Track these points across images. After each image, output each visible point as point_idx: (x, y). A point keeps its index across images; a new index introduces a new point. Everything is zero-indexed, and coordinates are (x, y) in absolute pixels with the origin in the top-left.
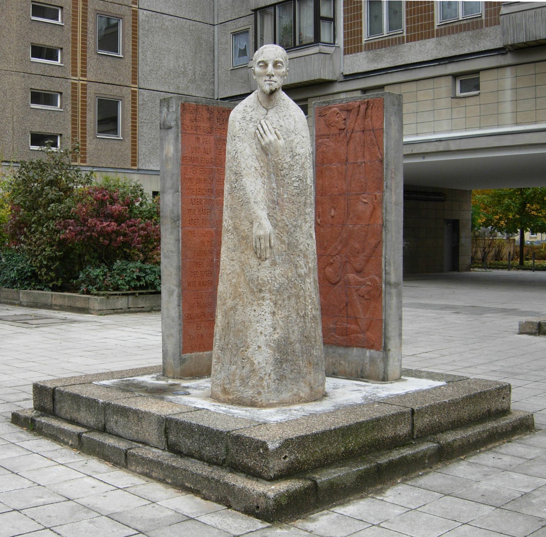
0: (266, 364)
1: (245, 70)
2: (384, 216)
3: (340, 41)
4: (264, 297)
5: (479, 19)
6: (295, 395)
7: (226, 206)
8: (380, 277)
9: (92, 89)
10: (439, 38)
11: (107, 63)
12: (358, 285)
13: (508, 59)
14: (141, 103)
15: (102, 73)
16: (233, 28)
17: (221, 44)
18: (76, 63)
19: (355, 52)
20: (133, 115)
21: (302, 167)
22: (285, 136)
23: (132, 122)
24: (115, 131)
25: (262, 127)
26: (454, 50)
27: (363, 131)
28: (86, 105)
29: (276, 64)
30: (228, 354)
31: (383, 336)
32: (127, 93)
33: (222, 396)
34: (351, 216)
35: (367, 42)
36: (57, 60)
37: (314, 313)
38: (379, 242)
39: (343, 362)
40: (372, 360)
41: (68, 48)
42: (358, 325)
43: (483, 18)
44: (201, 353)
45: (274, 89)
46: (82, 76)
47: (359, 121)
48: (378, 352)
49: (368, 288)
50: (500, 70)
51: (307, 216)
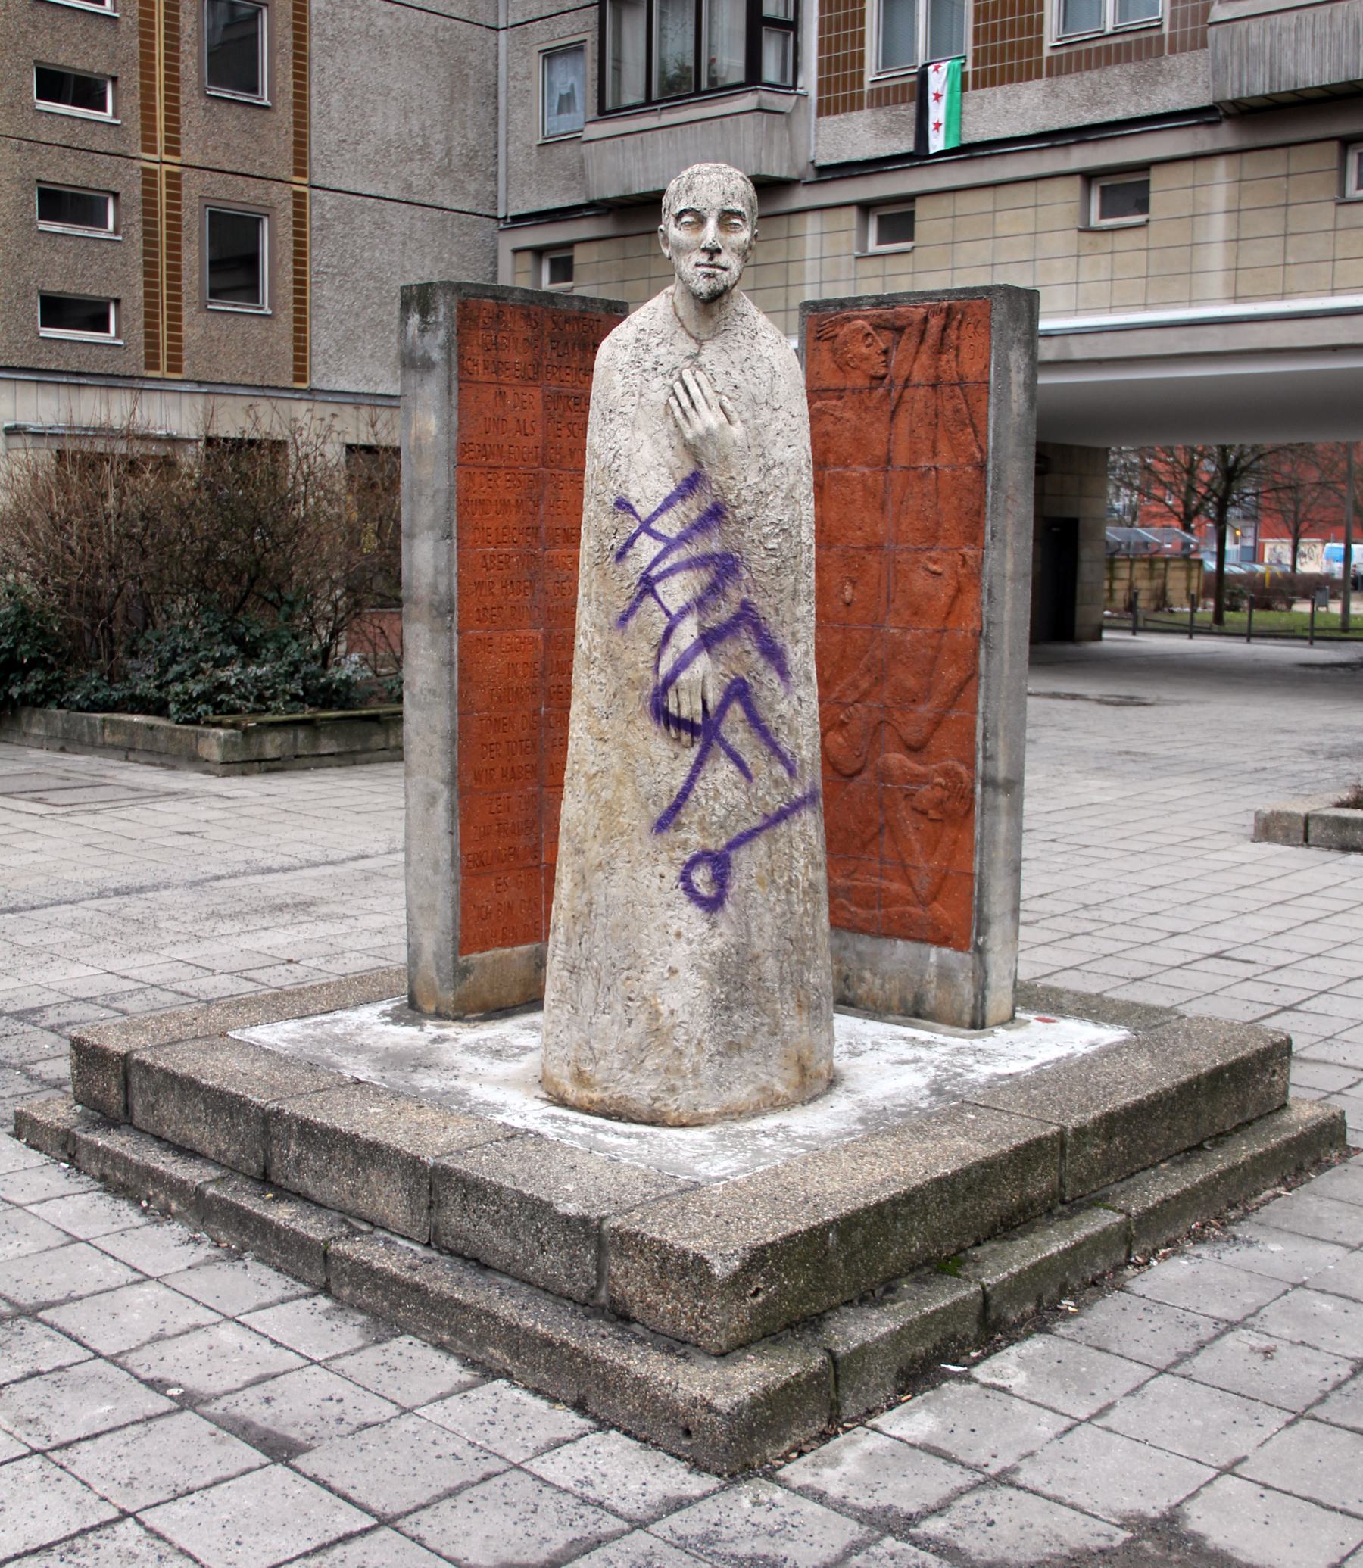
0: (691, 1014)
1: (574, 145)
2: (985, 609)
3: (809, 79)
4: (686, 842)
5: (1154, 33)
6: (763, 1090)
7: (587, 595)
8: (971, 766)
9: (194, 187)
10: (1054, 80)
11: (231, 119)
12: (909, 782)
13: (1224, 136)
14: (316, 223)
15: (216, 147)
16: (544, 38)
17: (514, 78)
18: (154, 118)
19: (844, 110)
20: (296, 253)
21: (789, 497)
22: (746, 415)
23: (296, 272)
24: (251, 291)
25: (687, 390)
26: (1088, 110)
27: (934, 386)
28: (178, 228)
29: (726, 218)
30: (589, 985)
31: (975, 915)
32: (281, 197)
33: (572, 1092)
34: (898, 604)
35: (876, 86)
36: (104, 109)
37: (811, 875)
38: (970, 677)
39: (867, 975)
40: (945, 975)
41: (132, 78)
42: (910, 883)
43: (1166, 30)
44: (508, 951)
45: (720, 287)
46: (168, 151)
47: (924, 358)
48: (960, 954)
49: (939, 793)
50: (1201, 165)
51: (799, 626)
